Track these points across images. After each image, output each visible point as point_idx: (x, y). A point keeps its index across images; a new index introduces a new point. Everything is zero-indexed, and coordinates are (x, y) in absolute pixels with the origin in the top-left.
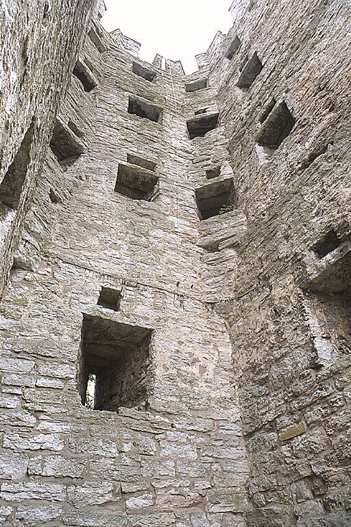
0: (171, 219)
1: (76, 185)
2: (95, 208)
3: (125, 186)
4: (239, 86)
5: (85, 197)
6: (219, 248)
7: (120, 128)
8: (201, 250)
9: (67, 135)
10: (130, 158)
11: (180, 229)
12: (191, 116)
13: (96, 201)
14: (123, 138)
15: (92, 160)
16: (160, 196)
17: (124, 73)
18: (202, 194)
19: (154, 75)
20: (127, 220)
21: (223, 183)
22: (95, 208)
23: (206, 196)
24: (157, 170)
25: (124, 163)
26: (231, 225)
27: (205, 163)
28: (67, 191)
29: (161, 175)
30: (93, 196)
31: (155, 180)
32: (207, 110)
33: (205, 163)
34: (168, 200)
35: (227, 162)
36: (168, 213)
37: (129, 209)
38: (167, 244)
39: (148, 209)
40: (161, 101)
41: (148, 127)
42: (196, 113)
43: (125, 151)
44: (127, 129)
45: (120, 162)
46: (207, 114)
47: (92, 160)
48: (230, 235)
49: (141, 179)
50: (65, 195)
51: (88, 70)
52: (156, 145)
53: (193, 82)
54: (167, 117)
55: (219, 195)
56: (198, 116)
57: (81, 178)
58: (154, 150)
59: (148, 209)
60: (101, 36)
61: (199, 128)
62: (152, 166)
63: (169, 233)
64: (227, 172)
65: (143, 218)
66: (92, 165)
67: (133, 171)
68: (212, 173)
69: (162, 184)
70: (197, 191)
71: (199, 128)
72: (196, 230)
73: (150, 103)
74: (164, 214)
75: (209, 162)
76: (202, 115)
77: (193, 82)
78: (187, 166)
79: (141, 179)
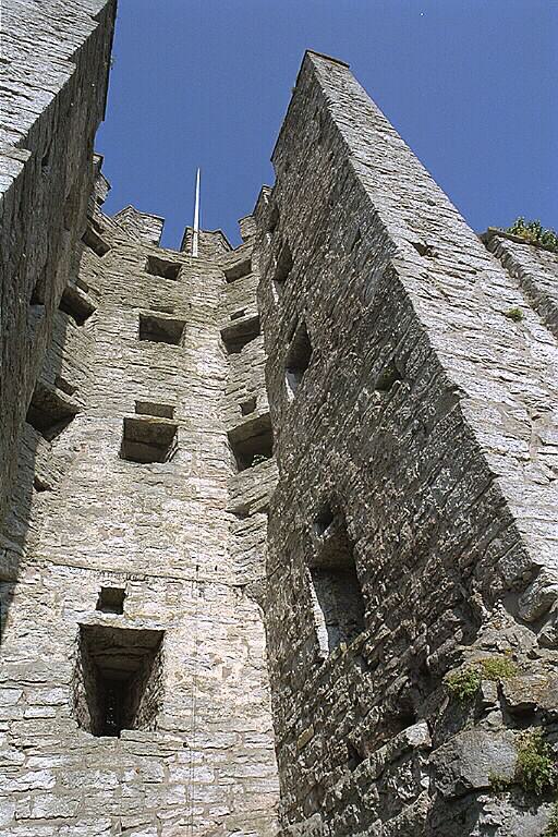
0: (191, 481)
10: (140, 407)
12: (227, 322)
13: (94, 477)
14: (130, 379)
16: (179, 452)
25: (131, 416)
30: (90, 470)
34: (189, 456)
40: (184, 310)
45: (125, 415)
46: (246, 318)
54: (191, 333)
56: (235, 322)
62: (168, 411)
68: (248, 407)
69: (181, 435)
71: (235, 340)
72: (226, 491)
75: (245, 391)
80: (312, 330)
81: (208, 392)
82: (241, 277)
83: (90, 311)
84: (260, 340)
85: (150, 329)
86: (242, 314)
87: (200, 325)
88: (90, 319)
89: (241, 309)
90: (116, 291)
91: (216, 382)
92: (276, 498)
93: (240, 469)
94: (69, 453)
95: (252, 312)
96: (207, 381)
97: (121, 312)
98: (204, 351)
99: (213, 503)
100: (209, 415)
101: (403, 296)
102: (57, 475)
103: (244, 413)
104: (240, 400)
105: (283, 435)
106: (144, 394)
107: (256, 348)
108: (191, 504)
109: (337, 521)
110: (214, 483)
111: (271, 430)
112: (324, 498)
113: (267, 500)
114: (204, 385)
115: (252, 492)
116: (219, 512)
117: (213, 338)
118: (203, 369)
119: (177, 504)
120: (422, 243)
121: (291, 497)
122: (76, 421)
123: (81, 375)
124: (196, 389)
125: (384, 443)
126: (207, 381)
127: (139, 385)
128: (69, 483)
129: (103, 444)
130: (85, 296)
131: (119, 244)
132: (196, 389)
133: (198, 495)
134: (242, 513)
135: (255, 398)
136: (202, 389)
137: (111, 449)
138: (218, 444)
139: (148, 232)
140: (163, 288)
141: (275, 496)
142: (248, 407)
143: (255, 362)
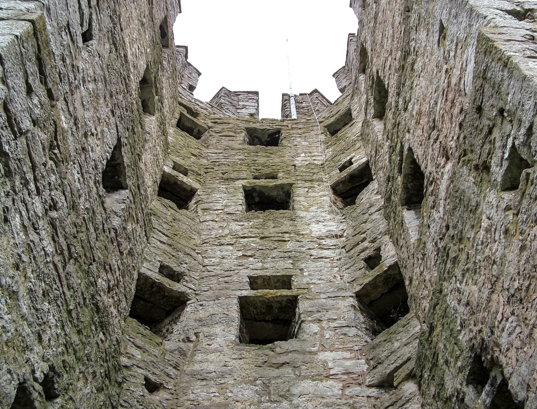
0: (323, 356)
1: (183, 353)
2: (212, 379)
3: (260, 321)
4: (378, 117)
5: (197, 367)
6: (395, 384)
7: (234, 240)
8: (374, 392)
9: (160, 287)
10: (254, 283)
11: (336, 368)
12: (336, 175)
13: (212, 368)
14: (240, 254)
15: (201, 305)
16: (303, 325)
17: (233, 152)
18: (367, 295)
19: (279, 132)
20: (258, 382)
21: (389, 272)
22: (212, 379)
23: (374, 295)
24: (296, 282)
25: (245, 293)
26: (403, 341)
27: (360, 247)
28: (170, 368)
29: (300, 291)
30: (207, 361)
31: (293, 301)
32: (353, 160)
33: (360, 247)
34: (315, 328)
35: (387, 238)
36: (316, 349)
37: (259, 363)
38: (321, 400)
39: (287, 352)
40: (288, 172)
41: (274, 222)
42: (342, 169)
43: (244, 274)
44: (245, 237)
45: (239, 293)
46: (355, 166)
47: (201, 305)
48: (405, 359)
49: (276, 305)
50: (168, 375)
51: (181, 177)
52: (289, 246)
53: (334, 118)
54: (300, 196)
55: (391, 291)
56: (345, 173)
57: (189, 340)
58: (286, 255)
59: (287, 352)
60: (195, 114)
61: (349, 189)
62: (285, 282)
63: (321, 380)
64: (389, 255)
65: (282, 370)
66: (202, 314)
67: (261, 299)
68: (373, 261)
69: (303, 306)
70: (358, 296)
71: (349, 189)
72: (363, 361)
73: (271, 183)
74: (310, 352)
75: (366, 244)
76: (348, 171)
77: (334, 118)
78: (340, 259)
79: (276, 305)
80: (418, 152)
81: (326, 253)
82: (344, 126)
83: (192, 192)
84: (374, 186)
85: (257, 199)
86: (350, 163)
87: (307, 184)
88: (193, 201)
89: (348, 158)
90: (216, 168)
91: (334, 241)
92: (420, 359)
93: (375, 333)
94: (182, 345)
95: (359, 159)
96: (323, 242)
97: (223, 187)
98: (317, 214)
99: (350, 378)
100: (331, 278)
101: (506, 63)
102: (172, 371)
103: (174, 168)
104: (364, 255)
105: (415, 283)
106: (256, 267)
107: (371, 196)
108: (324, 383)
109: (495, 378)
110: (348, 355)
111: (402, 282)
112: (472, 348)
113: (411, 365)
114: (321, 247)
115: (393, 358)
116: (358, 388)
117: (324, 195)
118: (317, 229)
119: (307, 386)
120: (518, 9)
121: (435, 355)
122: (188, 309)
123: (187, 259)
124: (313, 252)
125: (440, 142)
126: (323, 242)
127: (251, 259)
128: (186, 378)
129: (218, 329)
130: (185, 179)
131: (215, 123)
132: (313, 252)
133: (332, 372)
134: (386, 384)
135: (378, 249)
136: (320, 251)
137: (225, 333)
138: (346, 308)
139: (244, 107)
140: (264, 157)
141: (419, 358)
142: (373, 261)
143: (373, 210)
